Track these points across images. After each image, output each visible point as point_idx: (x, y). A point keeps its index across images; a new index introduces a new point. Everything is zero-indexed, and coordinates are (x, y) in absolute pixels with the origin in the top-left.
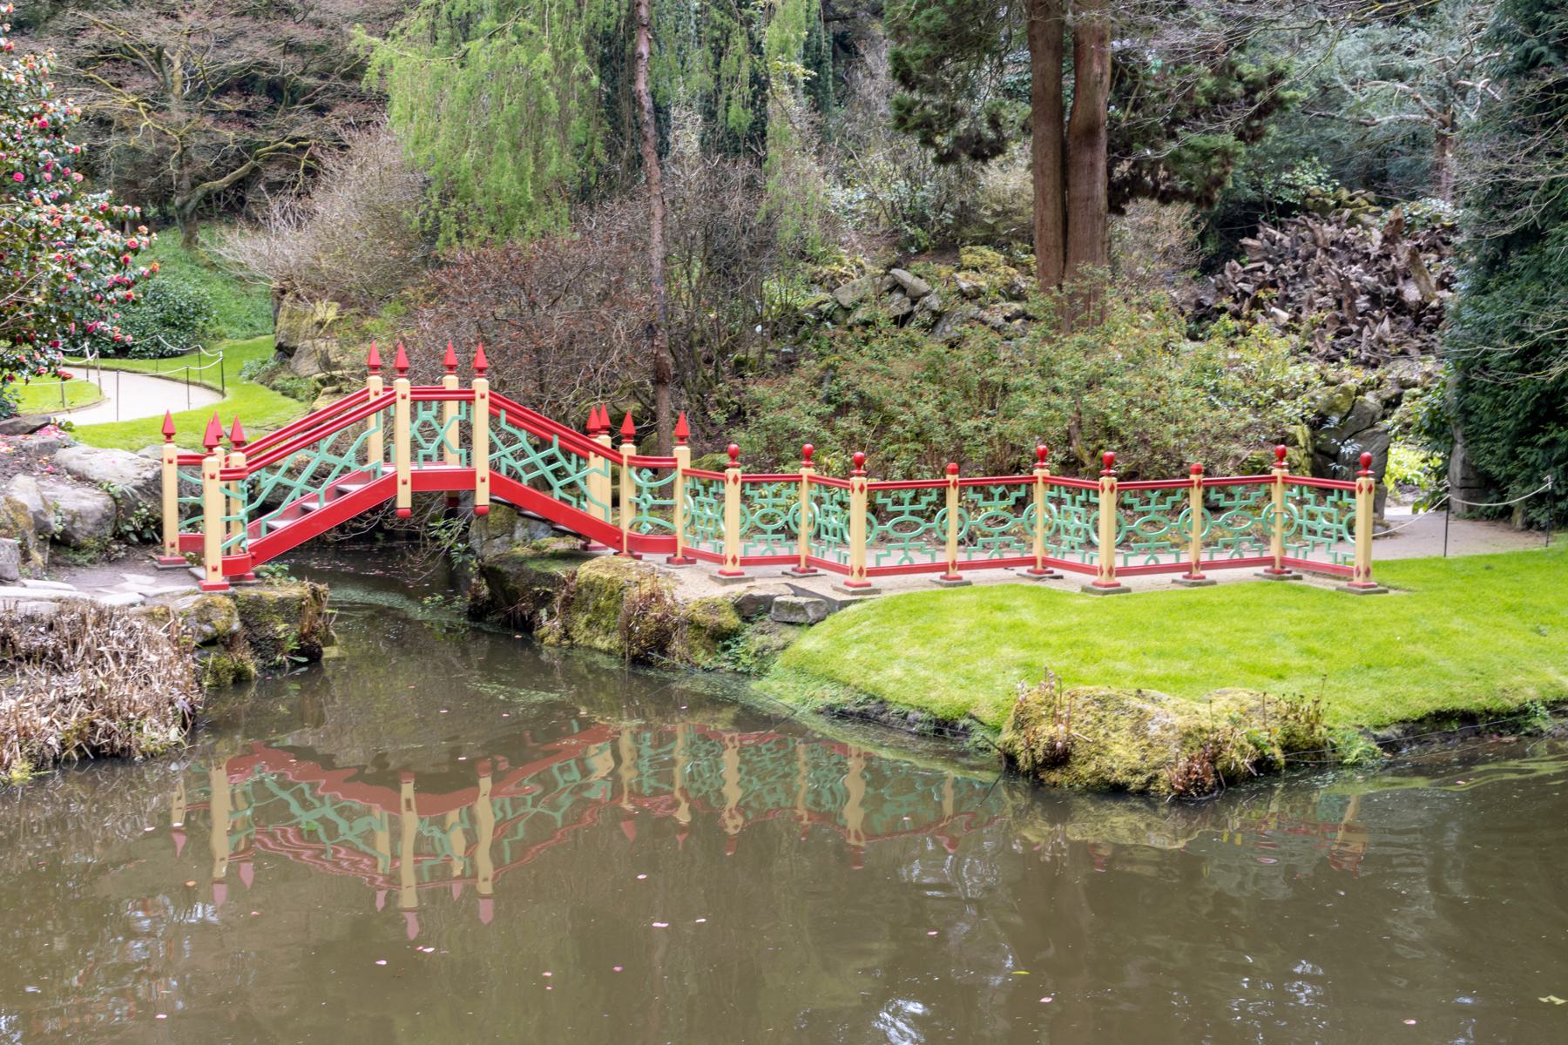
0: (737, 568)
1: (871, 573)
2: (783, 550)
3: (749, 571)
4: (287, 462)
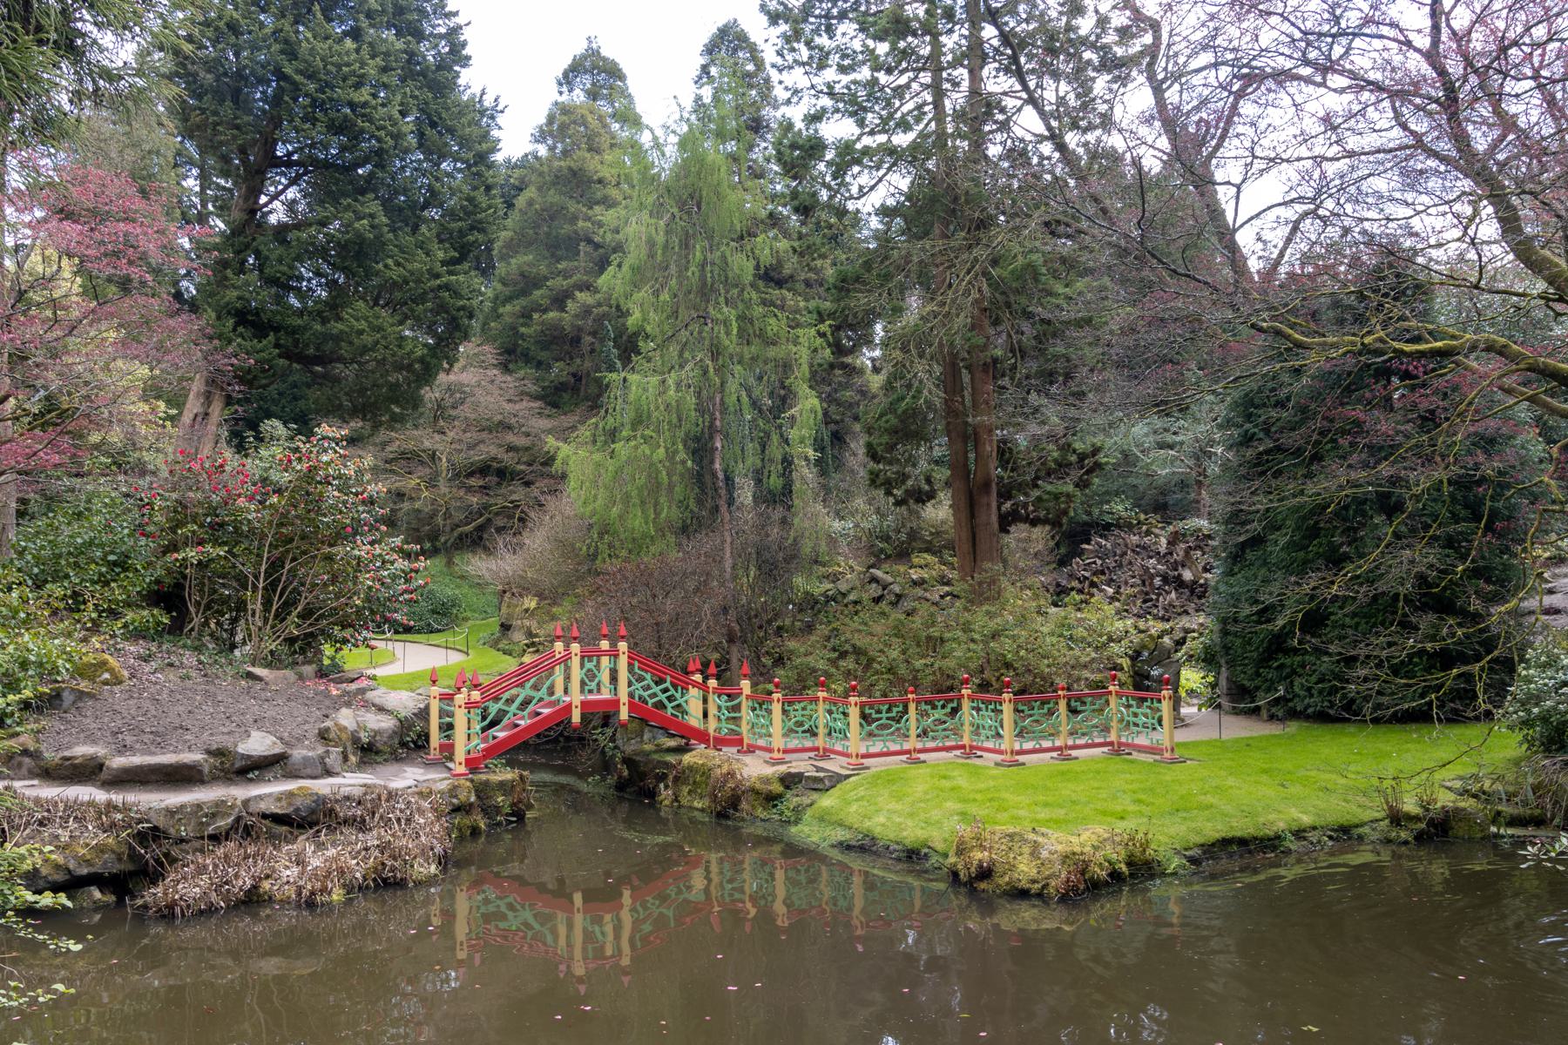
0: (781, 755)
1: (864, 756)
2: (808, 744)
3: (788, 757)
4: (506, 696)
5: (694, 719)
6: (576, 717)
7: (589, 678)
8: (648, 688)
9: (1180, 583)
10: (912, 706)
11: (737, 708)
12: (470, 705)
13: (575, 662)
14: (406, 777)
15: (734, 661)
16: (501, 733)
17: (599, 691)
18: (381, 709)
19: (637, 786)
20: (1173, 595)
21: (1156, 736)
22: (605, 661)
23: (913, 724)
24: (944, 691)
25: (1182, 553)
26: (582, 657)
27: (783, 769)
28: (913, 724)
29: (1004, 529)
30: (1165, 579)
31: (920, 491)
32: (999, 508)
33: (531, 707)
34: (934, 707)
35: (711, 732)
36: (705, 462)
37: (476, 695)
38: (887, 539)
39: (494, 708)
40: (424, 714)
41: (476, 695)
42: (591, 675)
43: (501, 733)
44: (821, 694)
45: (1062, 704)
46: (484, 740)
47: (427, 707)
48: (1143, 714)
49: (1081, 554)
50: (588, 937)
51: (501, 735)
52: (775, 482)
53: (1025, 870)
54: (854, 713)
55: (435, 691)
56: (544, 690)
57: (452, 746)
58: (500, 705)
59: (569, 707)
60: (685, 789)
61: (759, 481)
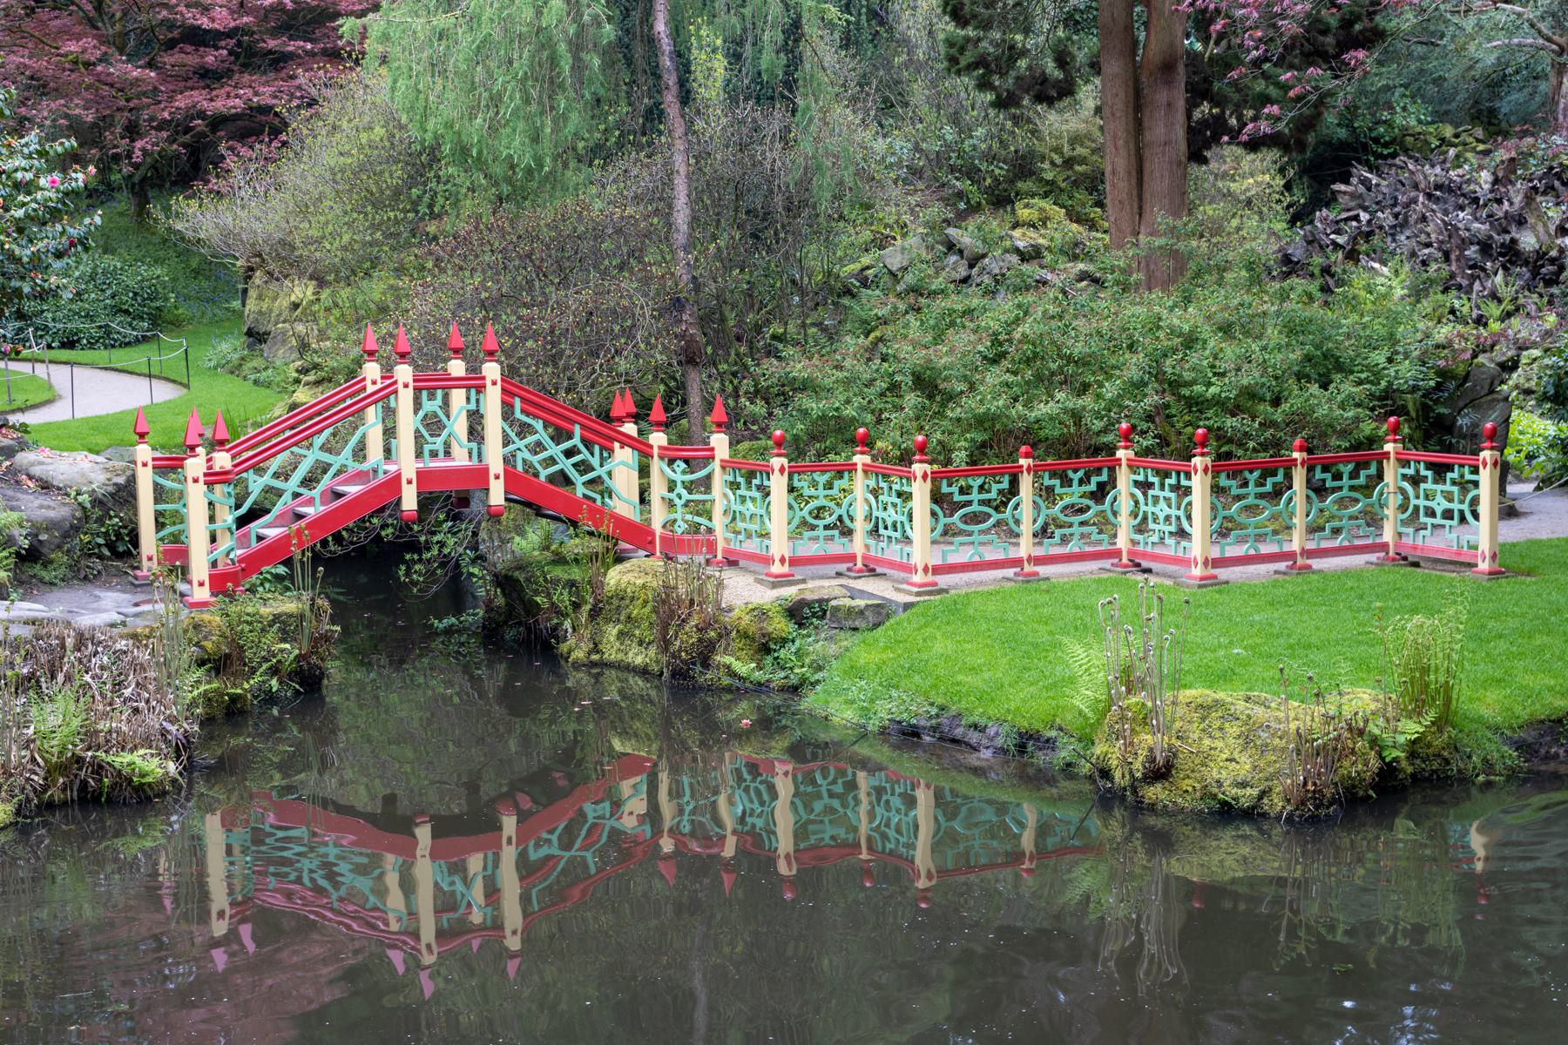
0: (786, 569)
1: (937, 570)
5: (624, 505)
6: (409, 501)
7: (431, 432)
8: (538, 447)
9: (1511, 255)
10: (1299, 476)
11: (706, 483)
12: (214, 478)
13: (405, 398)
14: (102, 608)
15: (695, 399)
16: (269, 529)
17: (447, 453)
18: (45, 486)
19: (521, 633)
20: (1499, 278)
21: (1465, 534)
22: (458, 396)
23: (1026, 512)
24: (1078, 455)
25: (1518, 200)
26: (418, 390)
27: (790, 592)
28: (1026, 512)
29: (1197, 157)
30: (1486, 247)
31: (1044, 80)
32: (1189, 117)
33: (326, 481)
34: (1067, 482)
35: (657, 526)
36: (636, 15)
37: (223, 460)
38: (971, 173)
39: (257, 485)
40: (125, 494)
41: (223, 460)
42: (434, 425)
43: (269, 529)
44: (860, 459)
45: (1299, 476)
46: (243, 541)
47: (132, 480)
48: (1439, 495)
49: (1331, 201)
50: (446, 903)
51: (273, 533)
52: (770, 60)
53: (1229, 767)
54: (920, 492)
55: (144, 452)
56: (348, 451)
57: (184, 554)
58: (267, 479)
59: (395, 482)
60: (612, 631)
61: (735, 57)
